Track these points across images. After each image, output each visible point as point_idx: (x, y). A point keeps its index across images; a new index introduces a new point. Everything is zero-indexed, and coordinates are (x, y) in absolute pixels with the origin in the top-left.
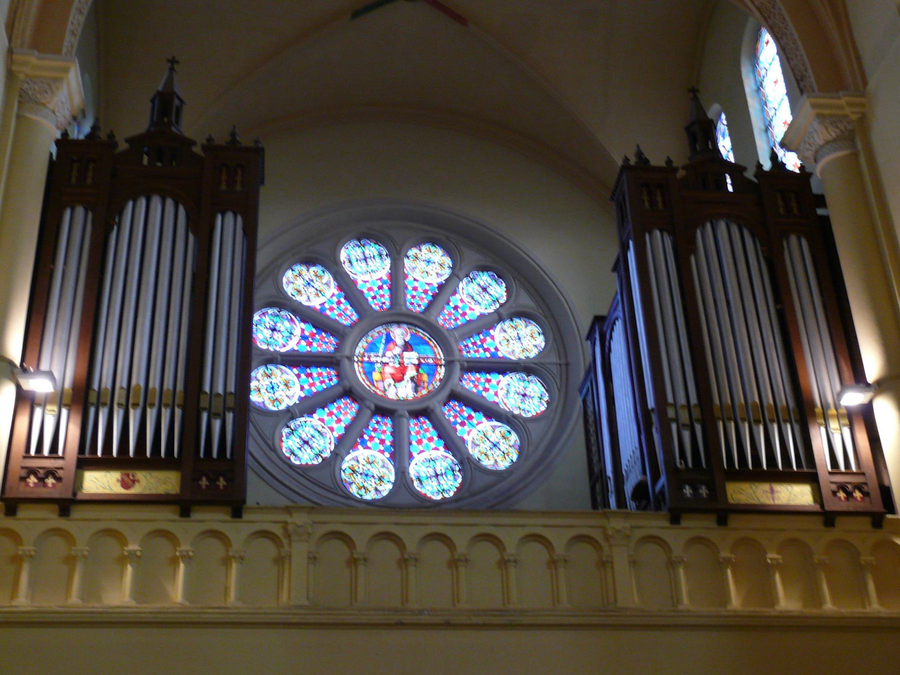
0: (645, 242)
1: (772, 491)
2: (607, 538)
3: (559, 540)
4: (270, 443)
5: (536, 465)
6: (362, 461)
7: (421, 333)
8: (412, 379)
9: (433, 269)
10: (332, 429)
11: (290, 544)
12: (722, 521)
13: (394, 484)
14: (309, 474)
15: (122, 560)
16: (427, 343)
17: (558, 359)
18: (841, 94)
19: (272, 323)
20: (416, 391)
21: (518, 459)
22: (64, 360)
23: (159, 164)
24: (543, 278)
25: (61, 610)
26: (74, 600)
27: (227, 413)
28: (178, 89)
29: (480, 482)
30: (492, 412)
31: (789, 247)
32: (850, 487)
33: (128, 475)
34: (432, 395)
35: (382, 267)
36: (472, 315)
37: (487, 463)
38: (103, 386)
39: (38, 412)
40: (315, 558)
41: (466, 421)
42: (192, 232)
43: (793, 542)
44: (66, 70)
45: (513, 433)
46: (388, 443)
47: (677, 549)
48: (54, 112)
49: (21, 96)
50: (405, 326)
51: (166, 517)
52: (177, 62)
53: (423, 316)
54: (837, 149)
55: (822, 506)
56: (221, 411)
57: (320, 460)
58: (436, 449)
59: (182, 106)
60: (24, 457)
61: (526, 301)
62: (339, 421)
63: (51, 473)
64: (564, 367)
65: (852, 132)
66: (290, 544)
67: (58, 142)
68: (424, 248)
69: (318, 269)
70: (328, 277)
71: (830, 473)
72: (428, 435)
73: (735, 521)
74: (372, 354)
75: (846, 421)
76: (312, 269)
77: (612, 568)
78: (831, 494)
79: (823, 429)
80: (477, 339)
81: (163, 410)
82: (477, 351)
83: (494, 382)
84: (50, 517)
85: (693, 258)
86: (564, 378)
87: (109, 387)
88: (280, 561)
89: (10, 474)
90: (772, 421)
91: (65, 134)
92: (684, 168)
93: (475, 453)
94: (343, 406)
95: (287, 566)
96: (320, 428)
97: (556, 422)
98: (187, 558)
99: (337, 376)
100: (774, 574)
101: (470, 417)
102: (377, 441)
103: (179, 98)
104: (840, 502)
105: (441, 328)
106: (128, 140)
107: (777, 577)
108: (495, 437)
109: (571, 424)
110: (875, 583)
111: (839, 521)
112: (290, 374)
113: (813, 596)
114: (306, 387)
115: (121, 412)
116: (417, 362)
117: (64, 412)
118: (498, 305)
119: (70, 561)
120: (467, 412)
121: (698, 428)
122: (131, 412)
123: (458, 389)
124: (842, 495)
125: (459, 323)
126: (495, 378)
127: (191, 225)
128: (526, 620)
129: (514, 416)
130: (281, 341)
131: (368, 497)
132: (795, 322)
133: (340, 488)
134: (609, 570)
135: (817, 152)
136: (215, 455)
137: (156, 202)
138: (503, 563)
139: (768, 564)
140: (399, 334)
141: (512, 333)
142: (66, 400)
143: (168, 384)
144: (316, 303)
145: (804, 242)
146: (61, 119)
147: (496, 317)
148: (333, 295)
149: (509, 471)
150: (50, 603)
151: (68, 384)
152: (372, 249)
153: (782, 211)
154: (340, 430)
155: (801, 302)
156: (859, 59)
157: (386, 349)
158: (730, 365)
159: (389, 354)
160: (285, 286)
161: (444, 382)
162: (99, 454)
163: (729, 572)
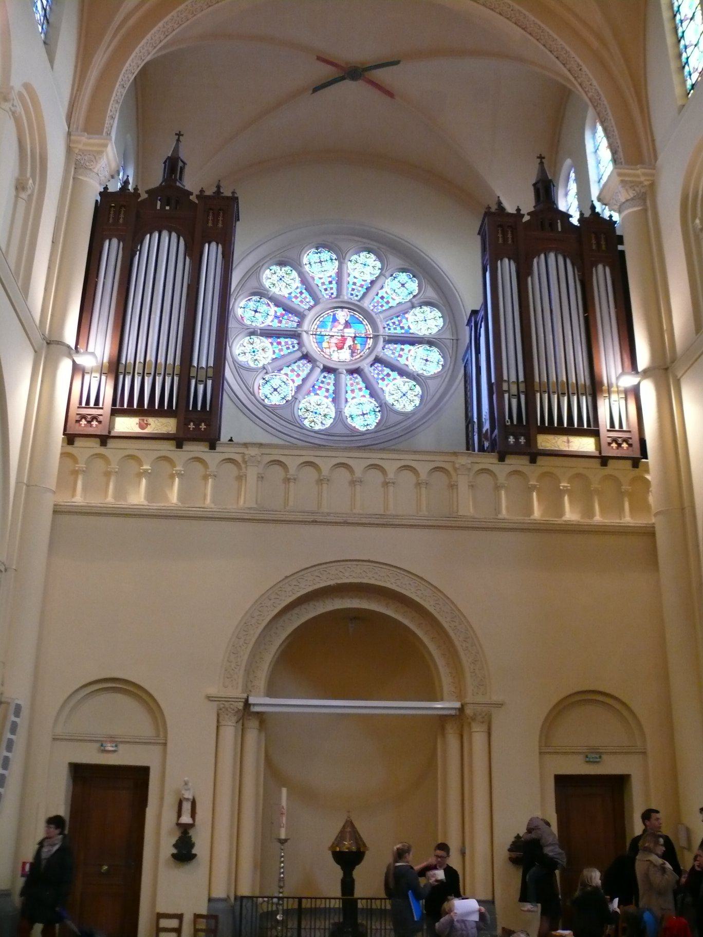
0: (497, 268)
1: (568, 442)
2: (455, 469)
3: (423, 469)
4: (251, 390)
5: (431, 410)
6: (313, 404)
7: (357, 315)
8: (350, 347)
9: (368, 270)
10: (293, 381)
11: (246, 467)
12: (533, 461)
13: (334, 419)
14: (277, 411)
15: (140, 475)
16: (362, 323)
17: (451, 336)
18: (638, 166)
19: (255, 306)
20: (352, 356)
21: (420, 404)
22: (104, 341)
23: (168, 208)
24: (443, 277)
25: (102, 505)
26: (110, 499)
27: (208, 381)
28: (183, 154)
29: (394, 419)
30: (403, 372)
31: (597, 273)
32: (620, 440)
33: (143, 420)
34: (363, 358)
35: (332, 268)
36: (393, 303)
37: (398, 407)
38: (128, 361)
39: (87, 377)
40: (262, 477)
41: (385, 377)
42: (188, 256)
43: (578, 476)
44: (106, 146)
45: (417, 386)
46: (331, 391)
47: (502, 478)
48: (98, 175)
49: (76, 164)
50: (347, 310)
51: (167, 448)
52: (182, 135)
53: (358, 303)
54: (629, 207)
55: (600, 453)
56: (204, 379)
57: (285, 401)
58: (364, 396)
59: (184, 166)
60: (78, 407)
61: (431, 294)
62: (298, 375)
63: (94, 418)
64: (455, 341)
65: (645, 193)
66: (246, 467)
67: (101, 194)
68: (361, 254)
69: (288, 268)
70: (294, 274)
71: (608, 431)
72: (359, 386)
73: (541, 460)
74: (323, 330)
75: (623, 396)
76: (283, 269)
77: (457, 488)
78: (607, 444)
79: (607, 401)
80: (395, 320)
81: (167, 377)
82: (395, 329)
83: (406, 351)
84: (94, 444)
85: (529, 279)
86: (455, 349)
87: (132, 362)
88: (240, 478)
89: (70, 418)
90: (573, 394)
91: (106, 188)
92: (529, 214)
93: (390, 400)
94: (301, 365)
95: (244, 481)
96: (285, 380)
97: (447, 380)
98: (180, 475)
99: (298, 344)
100: (564, 496)
101: (388, 375)
102: (324, 390)
103: (182, 161)
104: (612, 450)
105: (371, 312)
106: (147, 192)
107: (566, 498)
108: (405, 389)
109: (458, 381)
110: (630, 504)
111: (611, 462)
112: (266, 342)
113: (588, 511)
114: (277, 351)
115: (140, 378)
116: (353, 335)
117: (104, 377)
118: (411, 296)
119: (108, 474)
120: (387, 370)
121: (523, 397)
122: (146, 378)
123: (381, 355)
124: (614, 445)
125: (384, 308)
126: (407, 347)
127: (189, 251)
128: (397, 522)
129: (418, 375)
130: (261, 319)
131: (317, 428)
132: (596, 326)
133: (298, 422)
134: (455, 490)
135: (620, 206)
136: (199, 409)
137: (165, 234)
138: (386, 484)
139: (561, 490)
140: (342, 315)
141: (420, 317)
142: (105, 370)
143: (170, 360)
144: (285, 292)
145: (608, 270)
146: (103, 178)
147: (409, 304)
148: (297, 288)
149: (413, 413)
150: (95, 501)
151: (106, 360)
152: (326, 255)
153: (594, 247)
154: (298, 381)
155: (601, 314)
156: (653, 141)
157: (333, 327)
158: (548, 355)
159: (334, 330)
160: (264, 281)
161: (372, 349)
162: (125, 406)
163: (535, 494)
